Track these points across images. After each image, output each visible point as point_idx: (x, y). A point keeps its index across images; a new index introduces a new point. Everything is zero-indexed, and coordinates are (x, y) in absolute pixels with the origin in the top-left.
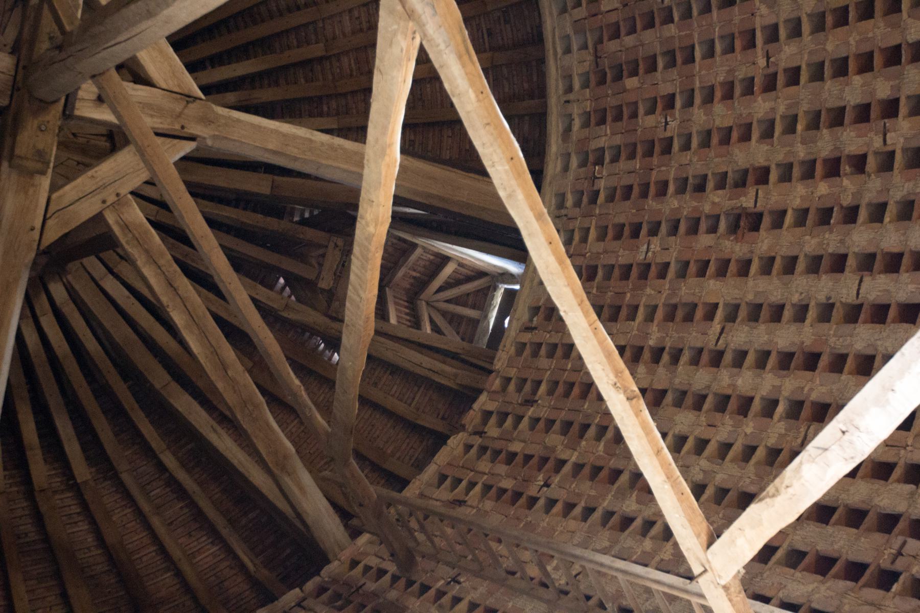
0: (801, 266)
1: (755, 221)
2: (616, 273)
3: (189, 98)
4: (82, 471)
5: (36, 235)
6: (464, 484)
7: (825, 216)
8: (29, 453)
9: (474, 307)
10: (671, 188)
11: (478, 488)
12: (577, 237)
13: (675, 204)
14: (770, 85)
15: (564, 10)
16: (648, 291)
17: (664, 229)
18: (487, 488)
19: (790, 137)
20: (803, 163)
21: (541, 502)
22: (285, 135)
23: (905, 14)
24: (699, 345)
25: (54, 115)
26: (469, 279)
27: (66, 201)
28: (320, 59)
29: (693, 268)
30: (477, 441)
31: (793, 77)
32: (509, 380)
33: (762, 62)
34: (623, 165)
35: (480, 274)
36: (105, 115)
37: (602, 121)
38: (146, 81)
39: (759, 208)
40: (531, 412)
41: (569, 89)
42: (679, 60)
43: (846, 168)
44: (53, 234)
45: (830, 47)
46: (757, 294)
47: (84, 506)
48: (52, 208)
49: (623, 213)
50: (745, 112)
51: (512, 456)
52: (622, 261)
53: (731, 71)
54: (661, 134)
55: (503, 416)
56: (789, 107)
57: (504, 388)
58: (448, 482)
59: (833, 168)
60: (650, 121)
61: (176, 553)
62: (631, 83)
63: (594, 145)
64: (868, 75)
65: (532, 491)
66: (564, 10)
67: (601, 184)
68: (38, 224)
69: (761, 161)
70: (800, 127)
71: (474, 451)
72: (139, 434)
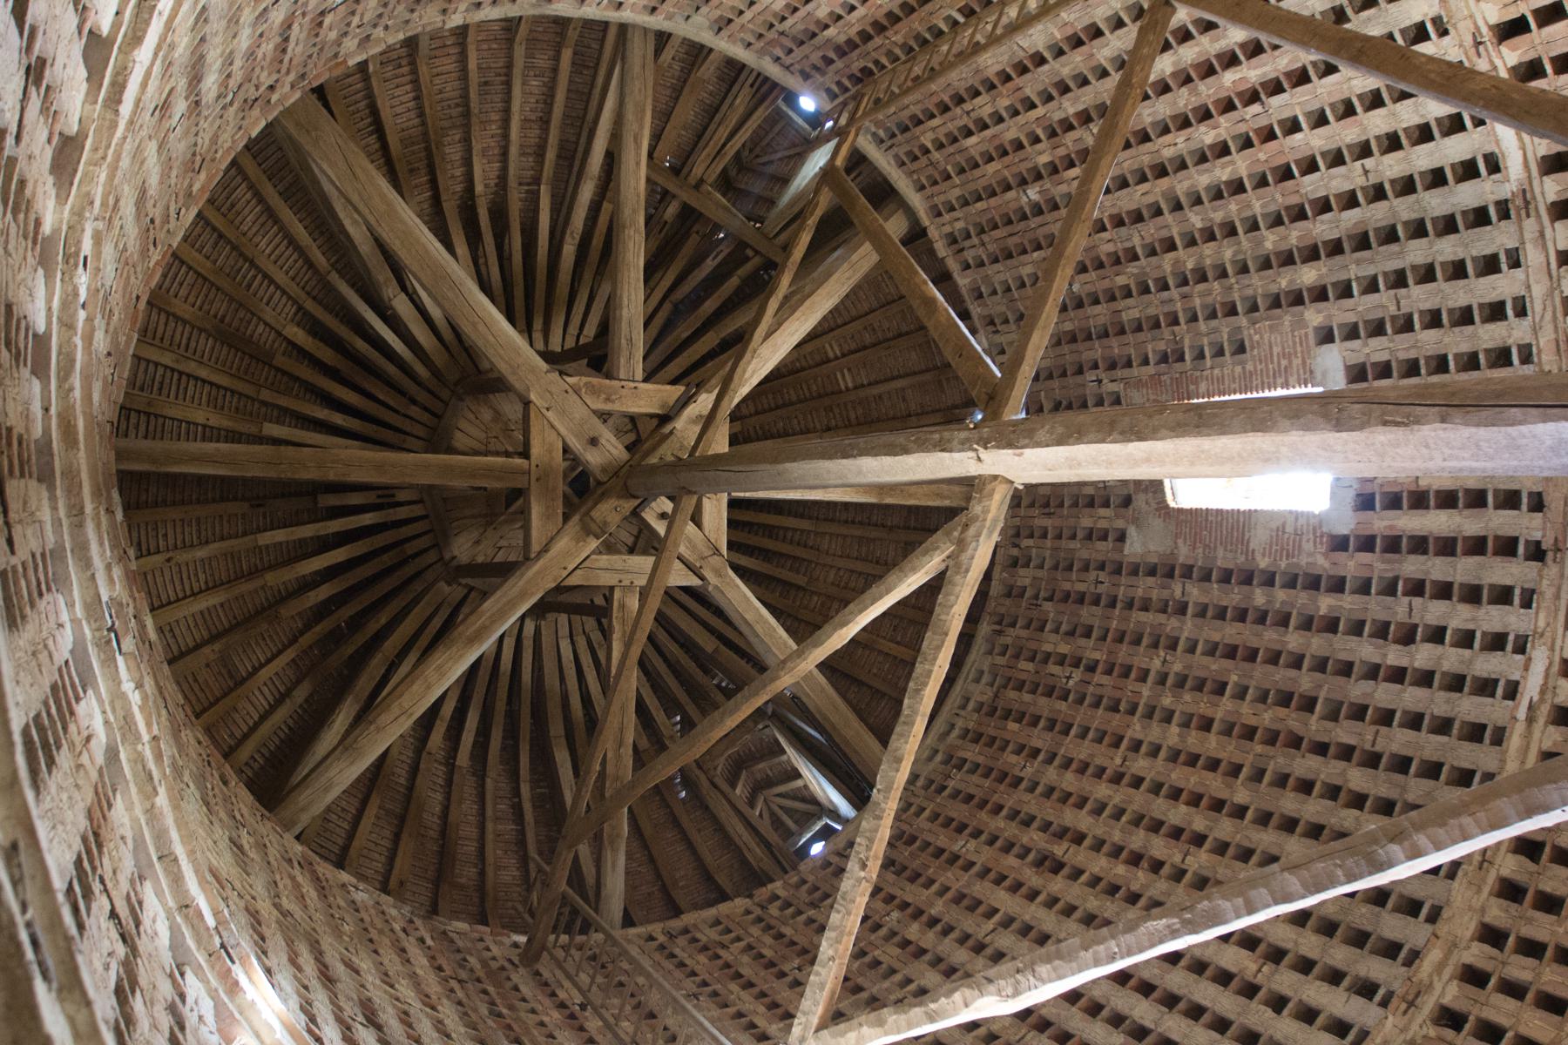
0: (1077, 914)
1: (1057, 867)
2: (931, 849)
3: (717, 552)
4: (463, 758)
5: (565, 573)
6: (733, 935)
7: (1113, 890)
8: (438, 722)
9: (796, 822)
10: (1004, 812)
11: (742, 944)
12: (913, 809)
13: (1002, 825)
14: (1117, 779)
15: (990, 652)
16: (949, 874)
17: (983, 837)
18: (750, 947)
19: (1113, 822)
20: (1114, 844)
21: (789, 979)
22: (761, 616)
23: (1239, 781)
24: (970, 931)
25: (628, 505)
26: (804, 800)
27: (597, 565)
28: (799, 588)
29: (992, 875)
30: (758, 911)
31: (1137, 782)
32: (804, 882)
33: (1118, 761)
34: (975, 778)
35: (814, 801)
36: (660, 528)
37: (976, 741)
38: (699, 525)
39: (1065, 859)
40: (811, 913)
41: (963, 707)
42: (1057, 728)
43: (1145, 864)
44: (574, 580)
45: (1173, 776)
46: (1033, 917)
47: (449, 782)
48: (586, 564)
49: (958, 811)
50: (1088, 788)
51: (780, 936)
52: (939, 843)
53: (1092, 756)
54: (1017, 772)
55: (788, 905)
56: (1124, 801)
57: (798, 886)
58: (720, 928)
59: (1135, 859)
60: (1013, 759)
61: (490, 858)
62: (1013, 726)
63: (962, 754)
64: (1193, 809)
65: (786, 968)
66: (990, 652)
67: (951, 784)
68: (571, 567)
69: (1083, 827)
70: (1124, 819)
71: (751, 917)
72: (518, 762)
